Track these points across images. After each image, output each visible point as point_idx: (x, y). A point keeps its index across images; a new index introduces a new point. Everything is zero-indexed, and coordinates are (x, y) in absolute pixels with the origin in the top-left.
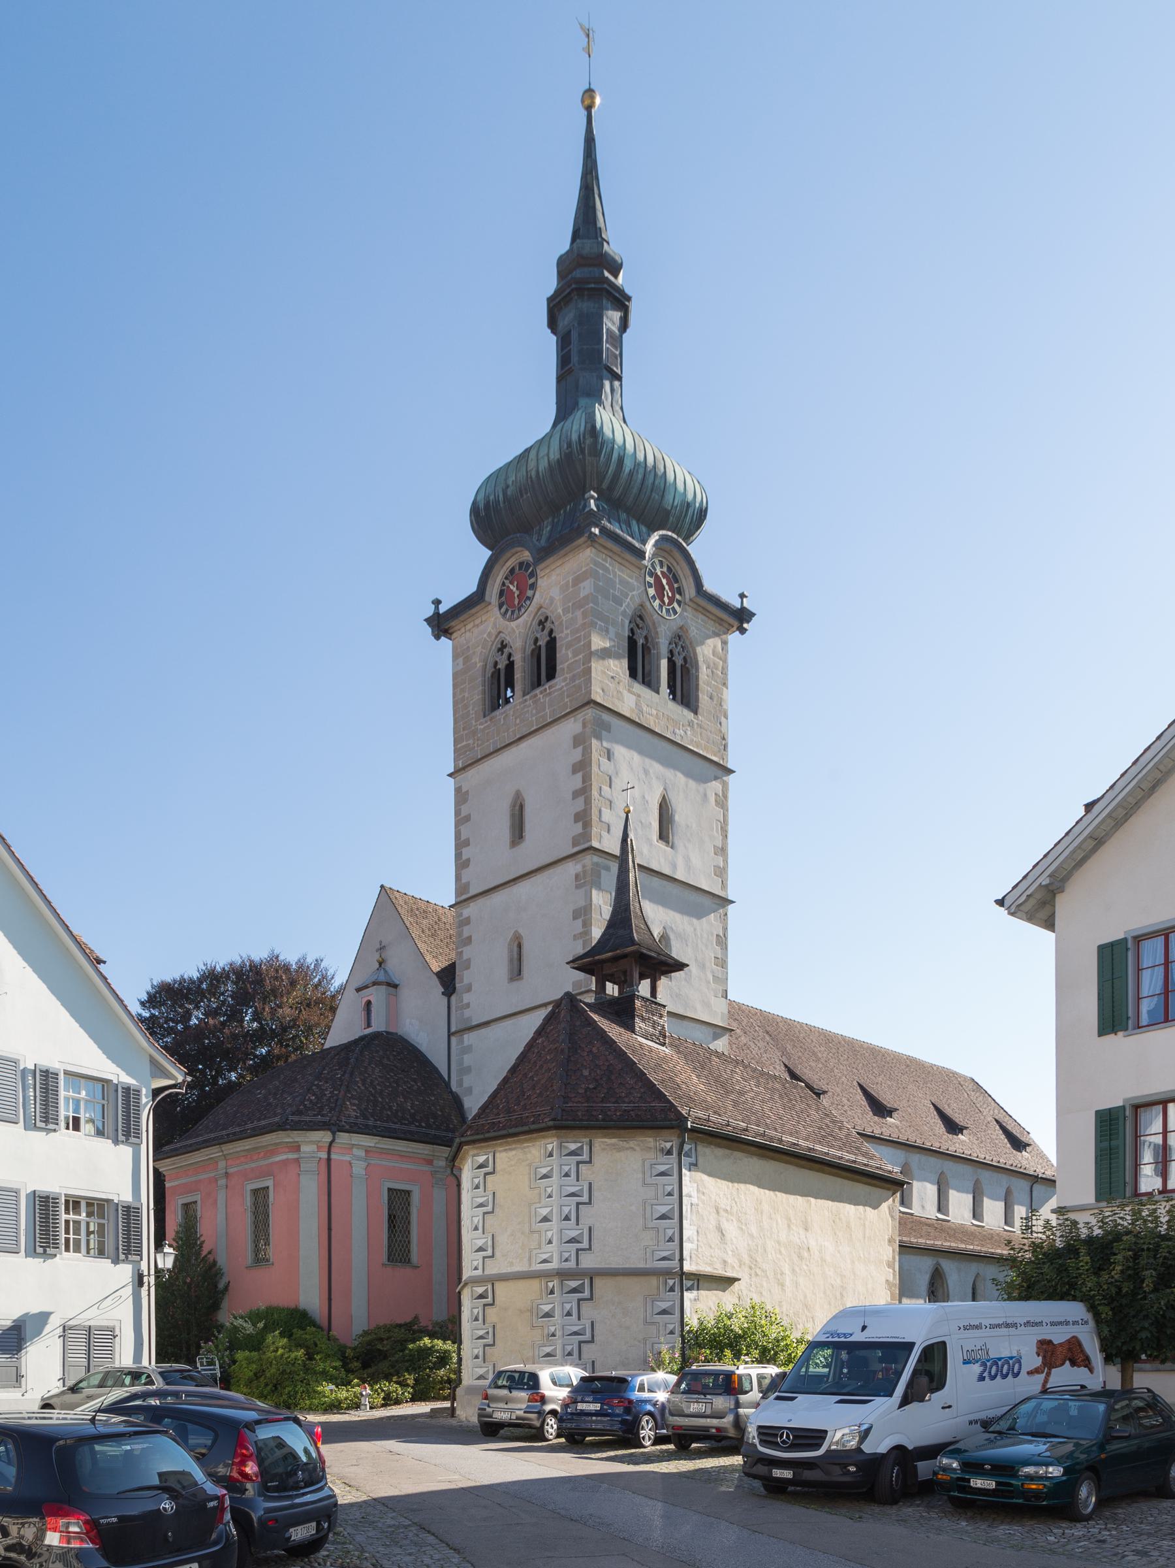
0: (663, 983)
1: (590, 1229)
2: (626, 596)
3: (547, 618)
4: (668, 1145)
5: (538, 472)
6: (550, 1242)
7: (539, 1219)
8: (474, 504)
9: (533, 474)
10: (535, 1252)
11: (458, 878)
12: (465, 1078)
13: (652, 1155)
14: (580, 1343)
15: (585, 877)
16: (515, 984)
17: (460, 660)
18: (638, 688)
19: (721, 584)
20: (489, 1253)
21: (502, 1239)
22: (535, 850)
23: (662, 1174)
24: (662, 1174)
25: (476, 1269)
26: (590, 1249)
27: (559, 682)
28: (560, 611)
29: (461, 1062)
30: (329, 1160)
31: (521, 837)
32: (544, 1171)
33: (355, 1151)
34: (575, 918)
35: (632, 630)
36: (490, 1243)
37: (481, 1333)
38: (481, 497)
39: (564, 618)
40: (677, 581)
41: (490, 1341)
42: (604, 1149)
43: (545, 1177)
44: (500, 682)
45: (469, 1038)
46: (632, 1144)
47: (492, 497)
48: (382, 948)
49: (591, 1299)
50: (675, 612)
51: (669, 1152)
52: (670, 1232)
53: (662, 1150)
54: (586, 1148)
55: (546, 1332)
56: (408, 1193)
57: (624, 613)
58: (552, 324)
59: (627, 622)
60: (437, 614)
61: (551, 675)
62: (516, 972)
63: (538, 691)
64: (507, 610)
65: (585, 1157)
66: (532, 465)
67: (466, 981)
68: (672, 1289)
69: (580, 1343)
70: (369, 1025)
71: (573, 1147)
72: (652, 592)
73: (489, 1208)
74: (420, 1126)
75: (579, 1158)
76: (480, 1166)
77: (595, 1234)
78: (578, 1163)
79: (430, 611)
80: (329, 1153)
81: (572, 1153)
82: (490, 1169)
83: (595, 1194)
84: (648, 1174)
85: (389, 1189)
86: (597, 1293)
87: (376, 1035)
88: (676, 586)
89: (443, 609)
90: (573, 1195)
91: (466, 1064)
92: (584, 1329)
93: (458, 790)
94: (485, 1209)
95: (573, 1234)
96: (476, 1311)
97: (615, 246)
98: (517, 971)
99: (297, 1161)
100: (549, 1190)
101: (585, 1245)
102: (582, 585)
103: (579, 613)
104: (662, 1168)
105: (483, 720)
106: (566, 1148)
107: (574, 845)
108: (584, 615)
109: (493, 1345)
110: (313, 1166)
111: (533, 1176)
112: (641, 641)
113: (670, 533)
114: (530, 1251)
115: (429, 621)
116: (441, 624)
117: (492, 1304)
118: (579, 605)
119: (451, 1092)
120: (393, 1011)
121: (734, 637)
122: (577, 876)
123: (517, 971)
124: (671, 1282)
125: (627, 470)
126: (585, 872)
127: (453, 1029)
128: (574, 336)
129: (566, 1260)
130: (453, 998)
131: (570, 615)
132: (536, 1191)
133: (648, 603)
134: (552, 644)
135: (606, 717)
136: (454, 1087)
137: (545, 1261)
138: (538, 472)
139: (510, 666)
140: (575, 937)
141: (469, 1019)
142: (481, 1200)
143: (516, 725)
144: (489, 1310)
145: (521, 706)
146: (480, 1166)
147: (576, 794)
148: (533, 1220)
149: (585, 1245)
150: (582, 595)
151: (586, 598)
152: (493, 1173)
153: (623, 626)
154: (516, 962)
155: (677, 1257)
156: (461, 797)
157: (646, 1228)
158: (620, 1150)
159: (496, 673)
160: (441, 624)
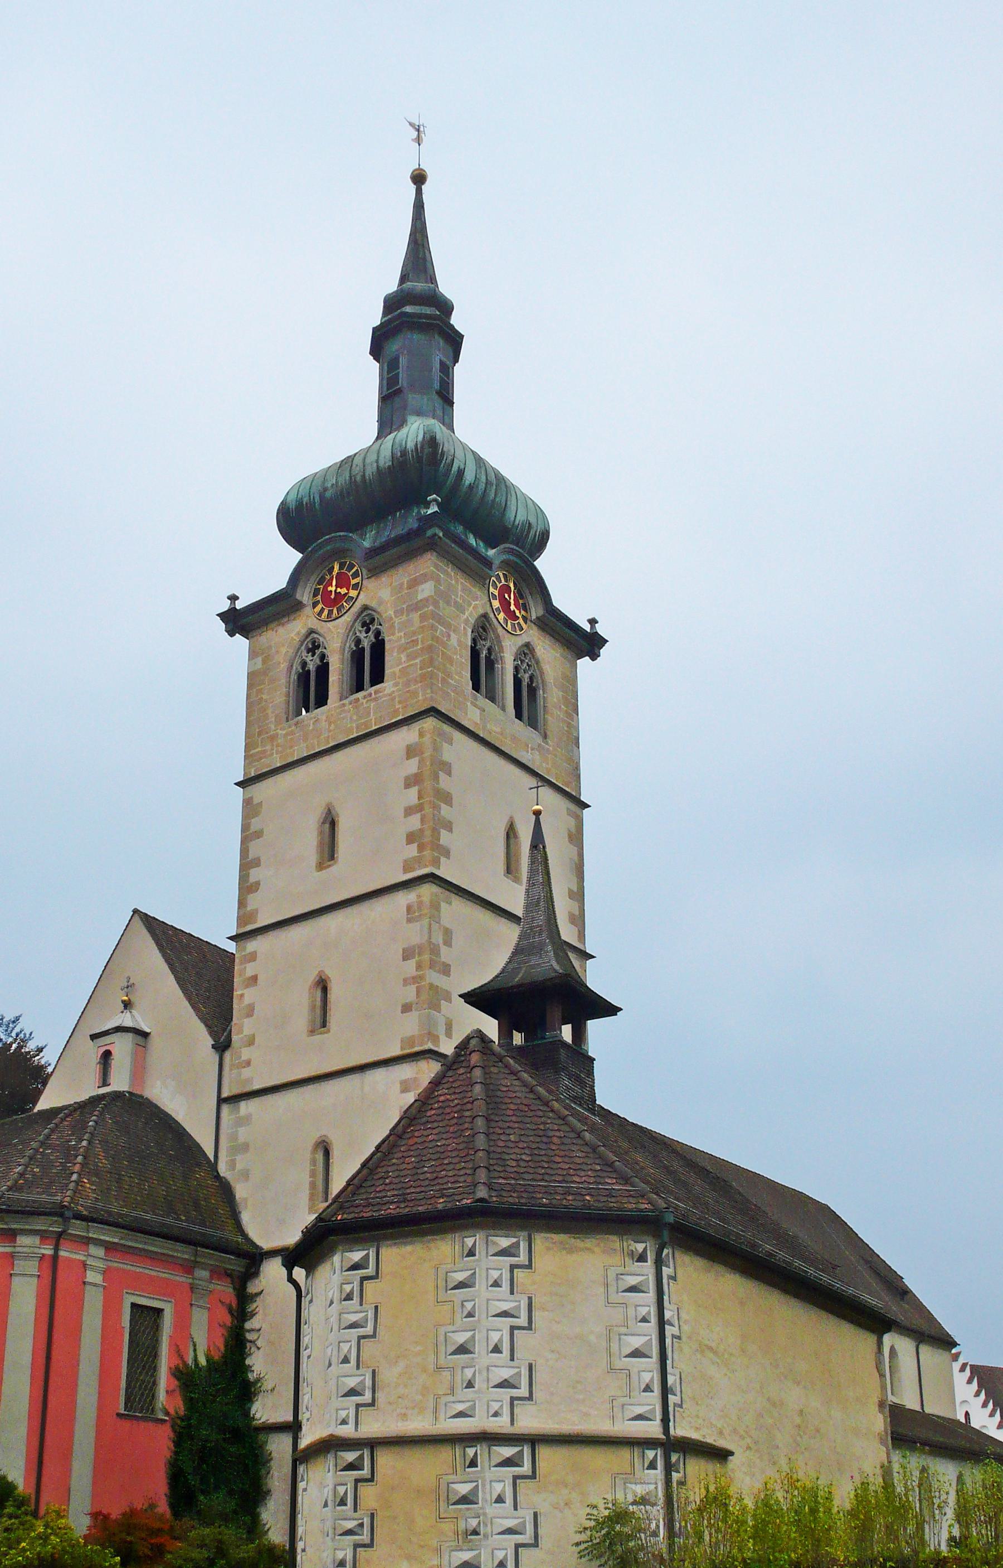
0: (594, 1027)
1: (530, 1366)
2: (470, 605)
3: (373, 620)
4: (640, 1247)
5: (364, 476)
6: (470, 1385)
7: (451, 1348)
8: (283, 503)
9: (359, 478)
10: (444, 1400)
11: (242, 903)
12: (238, 1158)
13: (617, 1259)
14: (517, 1546)
15: (420, 908)
16: (317, 1038)
17: (259, 660)
18: (483, 701)
19: (572, 601)
20: (367, 1397)
21: (388, 1375)
22: (348, 877)
23: (633, 1289)
24: (633, 1289)
25: (344, 1422)
26: (530, 1398)
27: (387, 686)
28: (391, 612)
29: (234, 1137)
30: (55, 1257)
31: (332, 857)
32: (460, 1277)
33: (93, 1250)
34: (405, 958)
35: (474, 641)
36: (368, 1383)
37: (350, 1525)
38: (292, 497)
39: (397, 621)
40: (522, 598)
41: (365, 1537)
42: (548, 1249)
43: (461, 1285)
44: (311, 689)
45: (245, 1107)
46: (590, 1242)
47: (305, 500)
48: (129, 987)
49: (533, 1476)
50: (521, 629)
51: (642, 1258)
52: (646, 1377)
53: (632, 1254)
54: (523, 1246)
55: (462, 1525)
56: (159, 1312)
57: (467, 621)
58: (377, 350)
59: (470, 631)
60: (233, 610)
61: (378, 677)
62: (319, 1021)
63: (360, 695)
64: (322, 610)
65: (523, 1258)
66: (356, 470)
67: (246, 1031)
68: (652, 1466)
69: (517, 1546)
70: (105, 1083)
71: (504, 1242)
72: (496, 604)
73: (369, 1329)
74: (178, 1219)
75: (514, 1260)
76: (355, 1267)
77: (537, 1377)
78: (513, 1267)
79: (225, 606)
80: (56, 1249)
81: (504, 1253)
82: (370, 1271)
83: (537, 1315)
84: (612, 1289)
85: (134, 1305)
86: (542, 1465)
87: (117, 1095)
88: (521, 602)
89: (239, 605)
90: (505, 1314)
91: (241, 1140)
92: (524, 1524)
93: (247, 802)
94: (361, 1331)
95: (506, 1374)
96: (341, 1490)
97: (446, 287)
98: (322, 1021)
99: (11, 1256)
100: (469, 1306)
101: (523, 1391)
102: (420, 588)
103: (415, 617)
104: (633, 1281)
105: (285, 725)
106: (495, 1243)
107: (406, 869)
108: (423, 618)
109: (371, 1545)
110: (32, 1267)
111: (441, 1284)
112: (484, 654)
113: (512, 546)
114: (437, 1397)
115: (222, 616)
116: (238, 621)
117: (371, 1480)
118: (416, 607)
119: (218, 1177)
120: (139, 1070)
121: (584, 663)
122: (409, 908)
123: (322, 1021)
124: (650, 1454)
125: (467, 483)
126: (420, 904)
127: (225, 1094)
128: (403, 361)
129: (496, 1414)
130: (228, 1055)
131: (404, 618)
132: (447, 1307)
133: (492, 616)
134: (379, 647)
135: (447, 728)
136: (223, 1169)
137: (461, 1414)
138: (364, 476)
139: (323, 670)
140: (406, 982)
141: (249, 1081)
142: (353, 1318)
143: (330, 731)
144: (364, 1490)
145: (341, 712)
146: (355, 1267)
147: (257, 863)
148: (442, 1348)
149: (523, 1391)
150: (419, 598)
151: (427, 600)
152: (375, 1277)
153: (466, 634)
154: (318, 1011)
155: (659, 1415)
156: (250, 809)
157: (612, 1369)
158: (571, 1251)
159: (304, 677)
160: (238, 621)
